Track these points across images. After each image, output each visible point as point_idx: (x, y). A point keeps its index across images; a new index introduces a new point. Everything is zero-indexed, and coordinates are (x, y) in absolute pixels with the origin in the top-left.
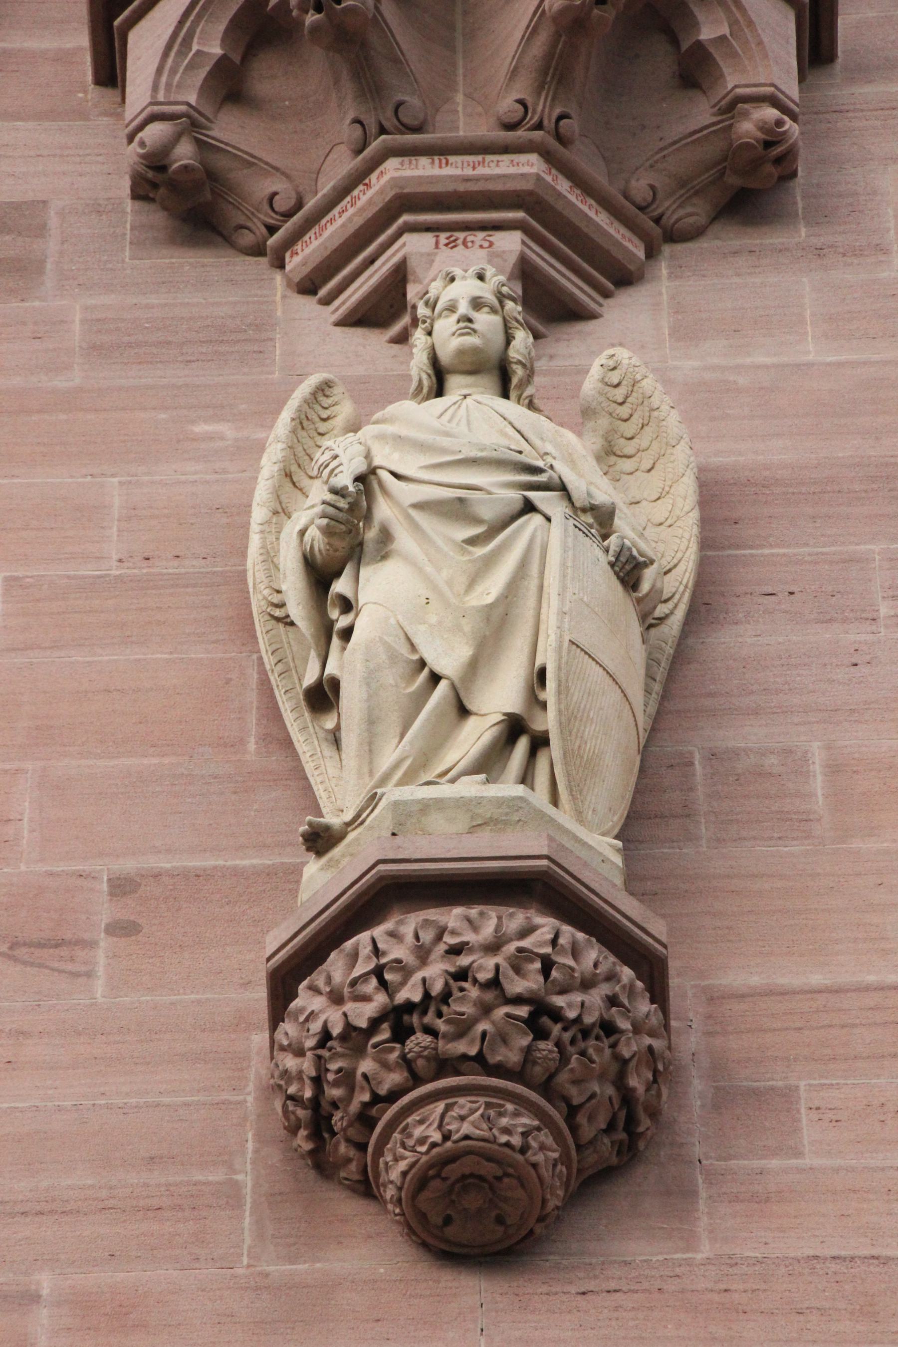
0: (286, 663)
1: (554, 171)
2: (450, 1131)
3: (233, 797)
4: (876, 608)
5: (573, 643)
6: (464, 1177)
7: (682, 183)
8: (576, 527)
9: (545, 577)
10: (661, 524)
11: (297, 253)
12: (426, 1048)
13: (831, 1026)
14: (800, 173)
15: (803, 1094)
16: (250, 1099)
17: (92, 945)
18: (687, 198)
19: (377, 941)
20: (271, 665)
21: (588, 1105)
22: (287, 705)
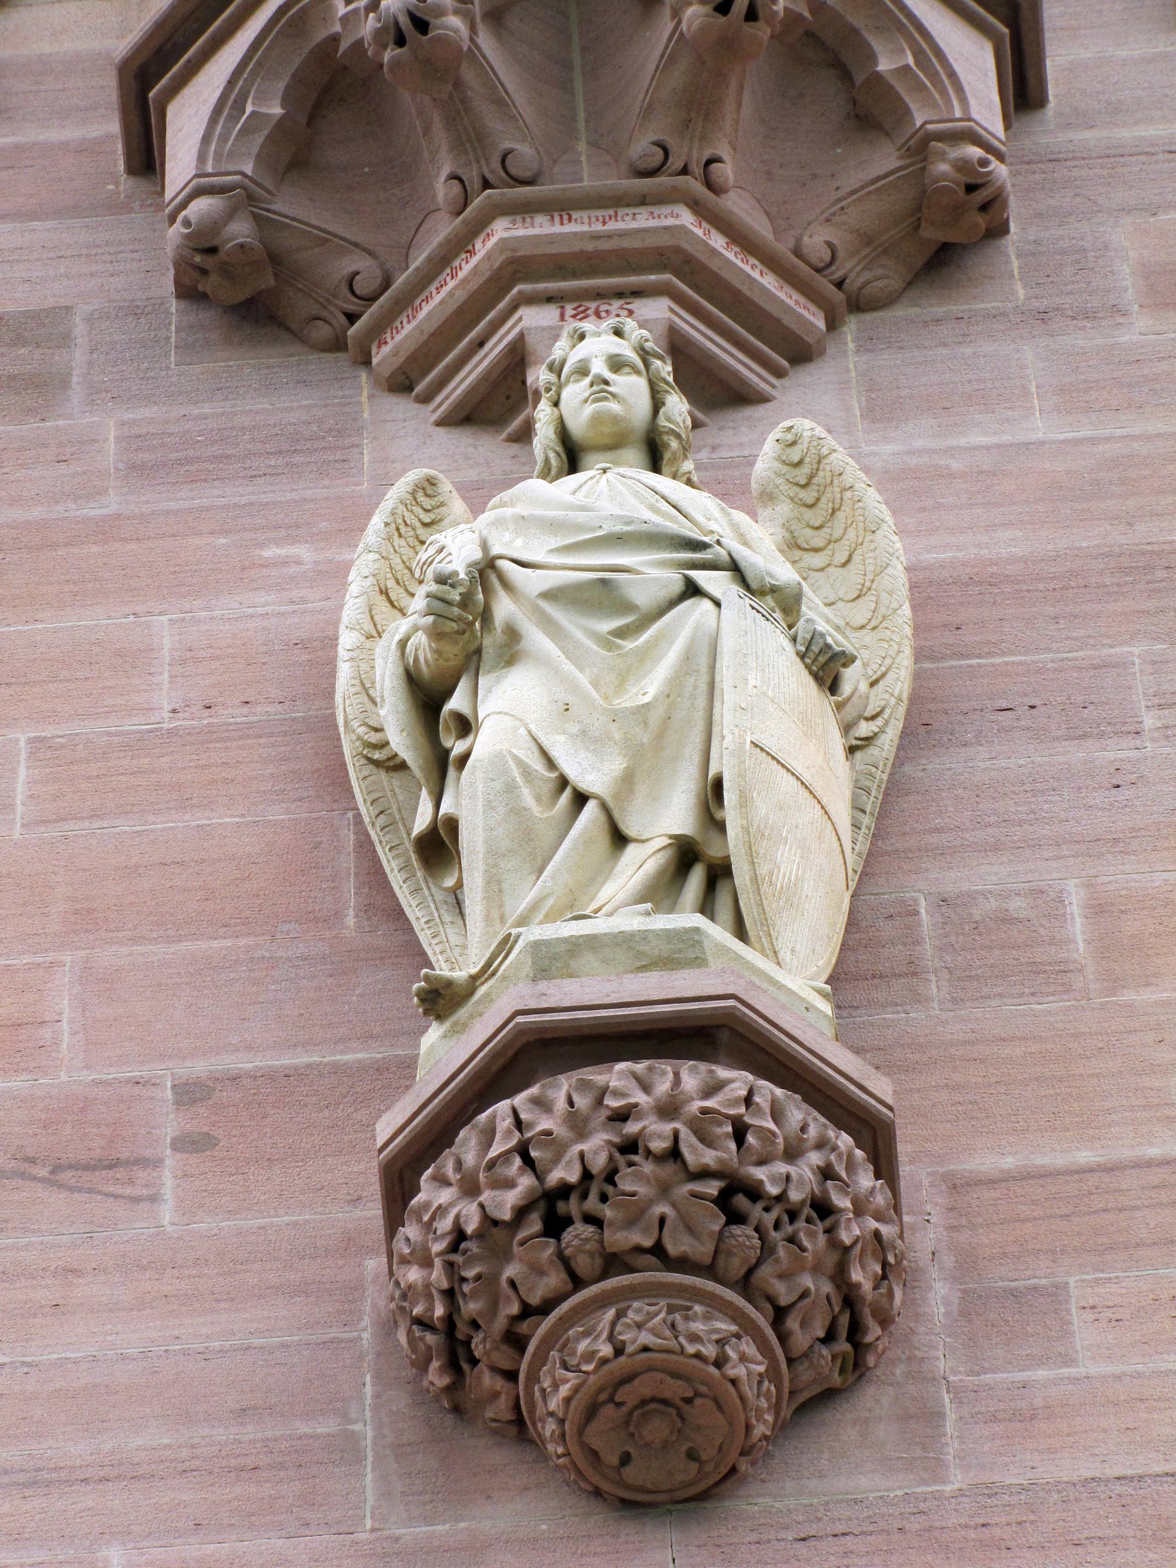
0: (390, 814)
1: (704, 224)
2: (624, 1343)
3: (329, 981)
4: (1140, 719)
5: (756, 746)
6: (644, 1402)
7: (867, 240)
8: (753, 608)
9: (717, 671)
10: (863, 627)
11: (386, 343)
12: (587, 1240)
13: (1105, 1210)
14: (1013, 227)
15: (1074, 1291)
16: (366, 1335)
17: (157, 1163)
18: (874, 258)
19: (519, 1110)
20: (370, 817)
21: (800, 1305)
22: (394, 864)
